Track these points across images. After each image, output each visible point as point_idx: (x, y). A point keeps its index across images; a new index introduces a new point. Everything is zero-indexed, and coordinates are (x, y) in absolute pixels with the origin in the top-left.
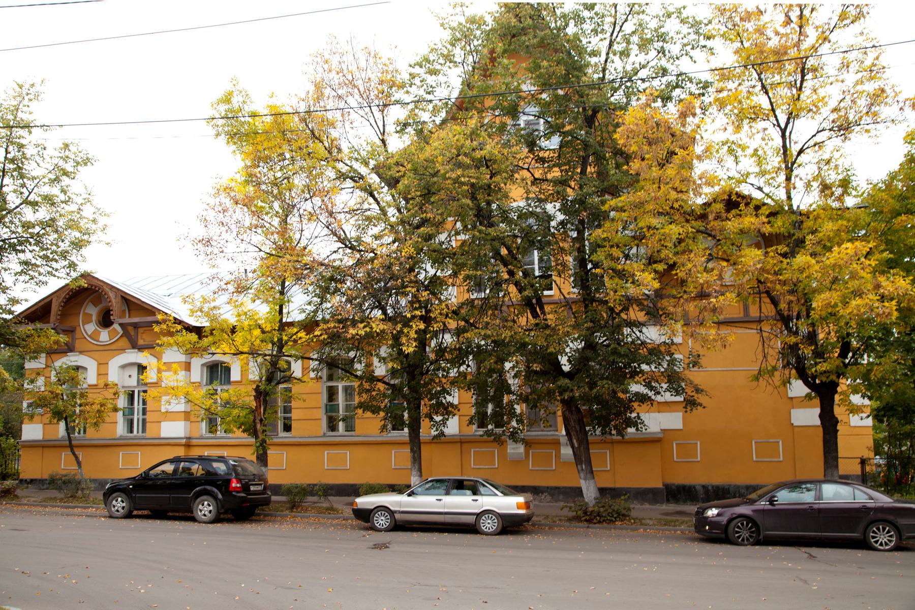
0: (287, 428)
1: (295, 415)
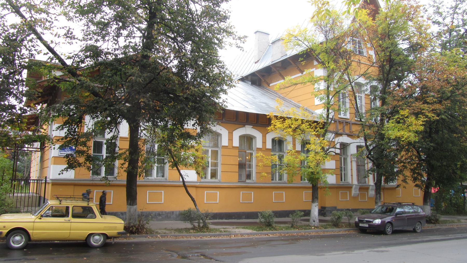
0: (214, 175)
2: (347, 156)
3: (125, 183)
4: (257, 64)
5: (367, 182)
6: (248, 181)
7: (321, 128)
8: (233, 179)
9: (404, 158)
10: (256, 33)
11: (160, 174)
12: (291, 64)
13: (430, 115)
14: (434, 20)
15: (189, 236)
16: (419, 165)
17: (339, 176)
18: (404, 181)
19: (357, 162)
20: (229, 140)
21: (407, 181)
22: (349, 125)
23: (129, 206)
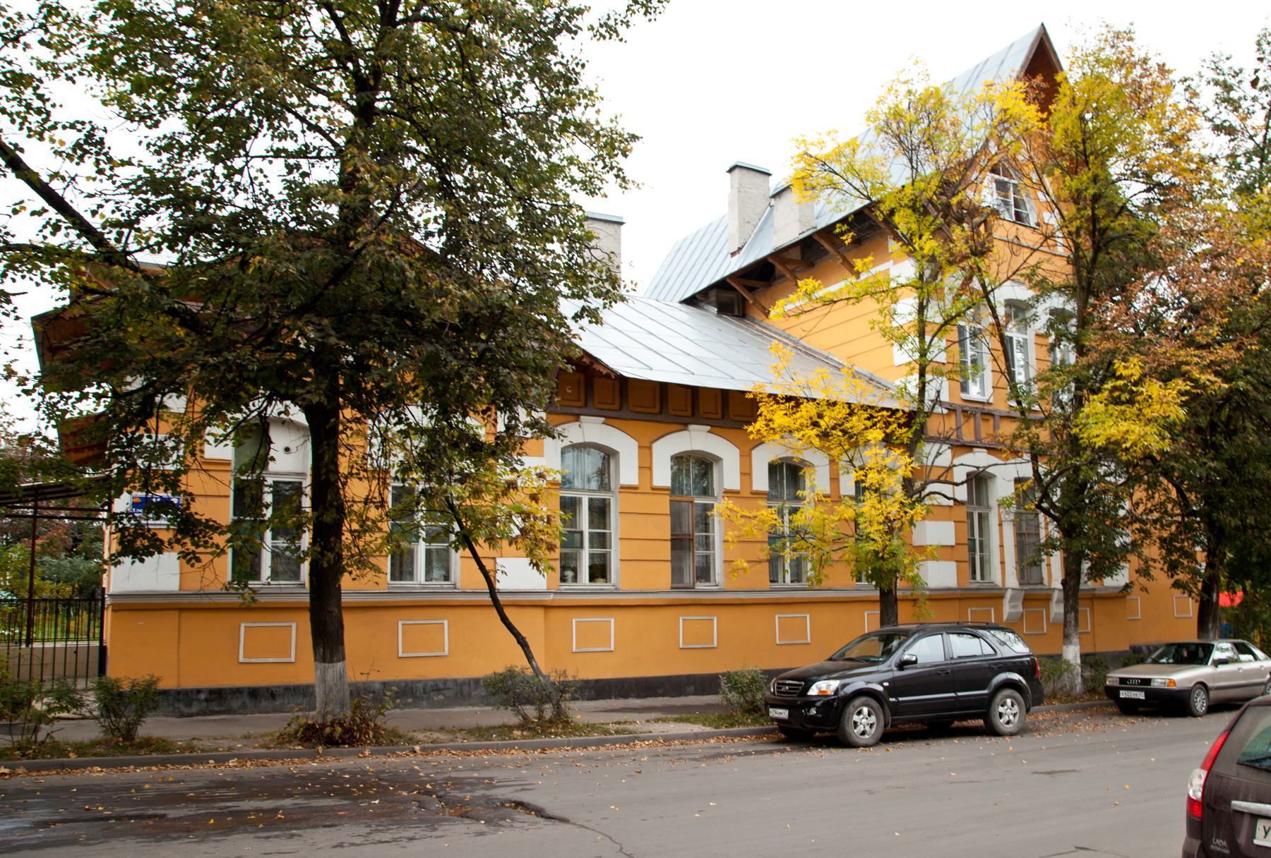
0: (599, 571)
1: (616, 554)
2: (989, 508)
3: (307, 599)
4: (737, 257)
5: (1046, 581)
6: (700, 586)
7: (900, 426)
8: (661, 577)
9: (1141, 508)
10: (731, 170)
11: (437, 573)
12: (826, 252)
13: (1205, 378)
14: (1218, 122)
15: (506, 746)
16: (1185, 528)
17: (967, 567)
18: (1145, 572)
19: (1017, 525)
20: (640, 467)
21: (1153, 572)
22: (991, 422)
23: (321, 665)
